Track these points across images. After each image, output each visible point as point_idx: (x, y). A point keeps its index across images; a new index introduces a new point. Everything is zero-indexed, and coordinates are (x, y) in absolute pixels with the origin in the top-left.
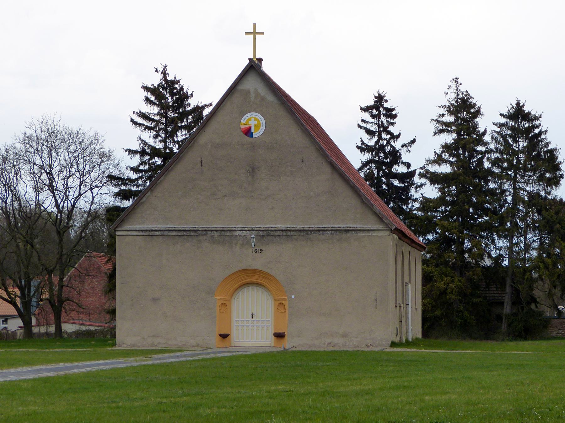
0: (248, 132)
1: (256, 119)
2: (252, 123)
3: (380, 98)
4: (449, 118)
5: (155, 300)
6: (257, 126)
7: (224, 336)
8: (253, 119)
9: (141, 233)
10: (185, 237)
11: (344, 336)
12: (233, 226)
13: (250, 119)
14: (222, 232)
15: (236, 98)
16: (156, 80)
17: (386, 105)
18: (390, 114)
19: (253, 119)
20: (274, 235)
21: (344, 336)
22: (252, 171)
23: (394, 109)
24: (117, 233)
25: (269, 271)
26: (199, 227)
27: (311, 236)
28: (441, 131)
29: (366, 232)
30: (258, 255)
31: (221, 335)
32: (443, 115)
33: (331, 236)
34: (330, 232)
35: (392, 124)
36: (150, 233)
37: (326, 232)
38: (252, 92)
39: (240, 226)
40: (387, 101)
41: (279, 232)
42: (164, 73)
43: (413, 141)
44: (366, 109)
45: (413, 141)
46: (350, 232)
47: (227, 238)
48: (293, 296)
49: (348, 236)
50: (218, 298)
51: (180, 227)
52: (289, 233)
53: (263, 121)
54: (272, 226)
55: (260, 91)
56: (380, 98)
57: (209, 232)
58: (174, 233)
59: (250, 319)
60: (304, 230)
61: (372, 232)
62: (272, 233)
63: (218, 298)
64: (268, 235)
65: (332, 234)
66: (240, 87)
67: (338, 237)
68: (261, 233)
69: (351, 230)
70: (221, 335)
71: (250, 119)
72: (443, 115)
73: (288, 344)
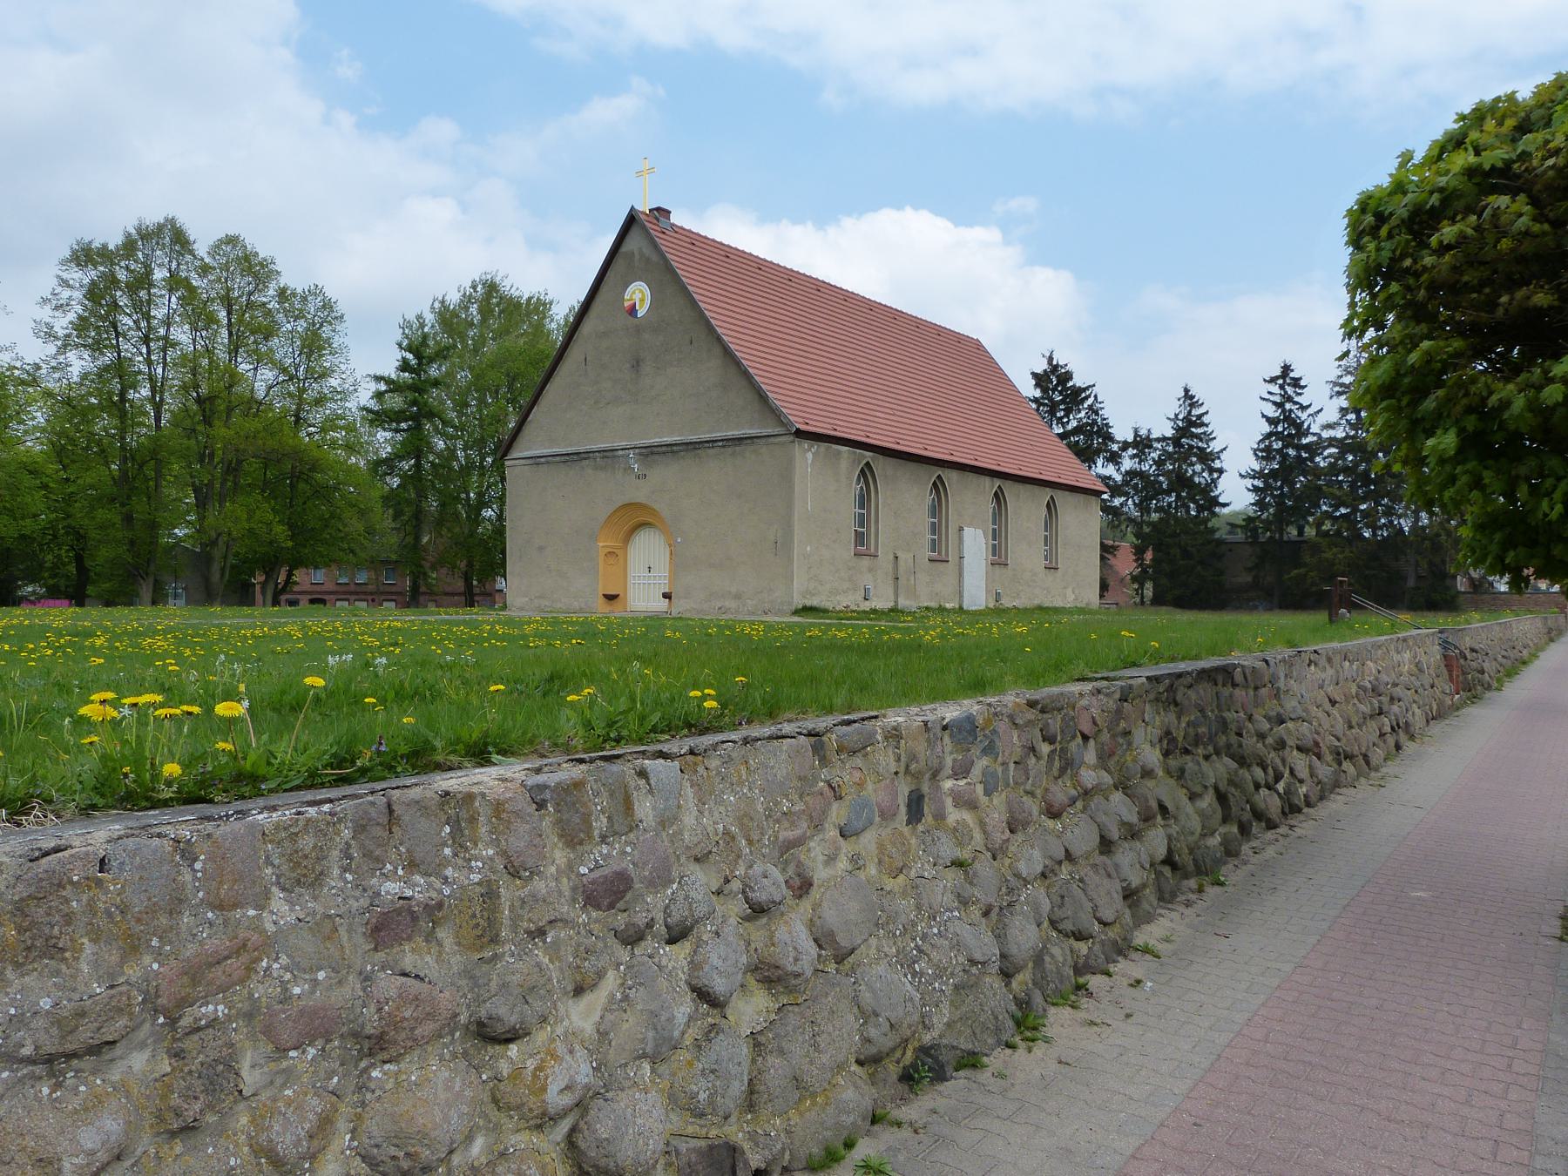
0: (632, 310)
1: (641, 291)
2: (637, 297)
3: (1286, 369)
4: (1348, 379)
5: (541, 549)
6: (642, 300)
7: (611, 598)
8: (637, 292)
9: (529, 462)
10: (569, 463)
11: (738, 597)
12: (616, 445)
13: (634, 292)
14: (605, 454)
15: (619, 263)
16: (1041, 366)
17: (1292, 375)
18: (1296, 383)
19: (637, 292)
20: (658, 453)
21: (738, 597)
22: (637, 364)
23: (1301, 378)
24: (507, 463)
25: (656, 507)
26: (582, 449)
27: (699, 451)
28: (1339, 394)
29: (764, 440)
30: (642, 481)
31: (606, 596)
32: (1341, 376)
33: (722, 450)
34: (720, 444)
35: (1300, 394)
36: (536, 460)
37: (715, 445)
38: (636, 253)
39: (624, 444)
40: (1292, 370)
41: (664, 449)
42: (1050, 359)
43: (1321, 410)
44: (1273, 380)
45: (1321, 410)
46: (746, 442)
47: (609, 461)
48: (679, 540)
49: (743, 447)
50: (601, 544)
51: (564, 451)
52: (675, 448)
53: (648, 292)
54: (656, 440)
55: (644, 250)
56: (1286, 369)
57: (591, 455)
58: (558, 459)
59: (647, 574)
60: (691, 443)
61: (772, 439)
62: (659, 449)
63: (601, 544)
64: (652, 453)
65: (723, 446)
66: (624, 249)
67: (730, 450)
68: (644, 451)
69: (746, 438)
70: (606, 596)
71: (634, 292)
72: (1341, 376)
73: (680, 607)
